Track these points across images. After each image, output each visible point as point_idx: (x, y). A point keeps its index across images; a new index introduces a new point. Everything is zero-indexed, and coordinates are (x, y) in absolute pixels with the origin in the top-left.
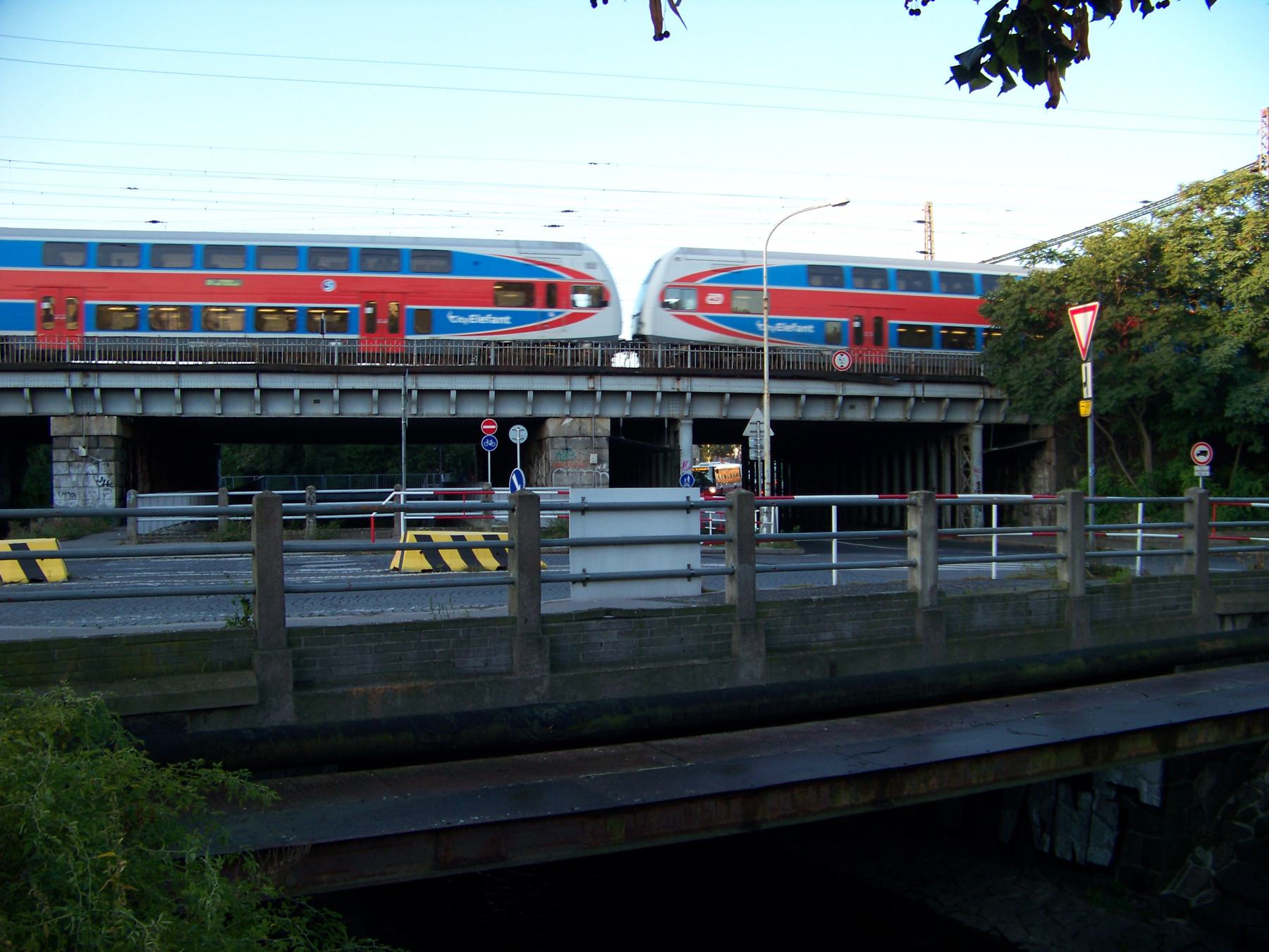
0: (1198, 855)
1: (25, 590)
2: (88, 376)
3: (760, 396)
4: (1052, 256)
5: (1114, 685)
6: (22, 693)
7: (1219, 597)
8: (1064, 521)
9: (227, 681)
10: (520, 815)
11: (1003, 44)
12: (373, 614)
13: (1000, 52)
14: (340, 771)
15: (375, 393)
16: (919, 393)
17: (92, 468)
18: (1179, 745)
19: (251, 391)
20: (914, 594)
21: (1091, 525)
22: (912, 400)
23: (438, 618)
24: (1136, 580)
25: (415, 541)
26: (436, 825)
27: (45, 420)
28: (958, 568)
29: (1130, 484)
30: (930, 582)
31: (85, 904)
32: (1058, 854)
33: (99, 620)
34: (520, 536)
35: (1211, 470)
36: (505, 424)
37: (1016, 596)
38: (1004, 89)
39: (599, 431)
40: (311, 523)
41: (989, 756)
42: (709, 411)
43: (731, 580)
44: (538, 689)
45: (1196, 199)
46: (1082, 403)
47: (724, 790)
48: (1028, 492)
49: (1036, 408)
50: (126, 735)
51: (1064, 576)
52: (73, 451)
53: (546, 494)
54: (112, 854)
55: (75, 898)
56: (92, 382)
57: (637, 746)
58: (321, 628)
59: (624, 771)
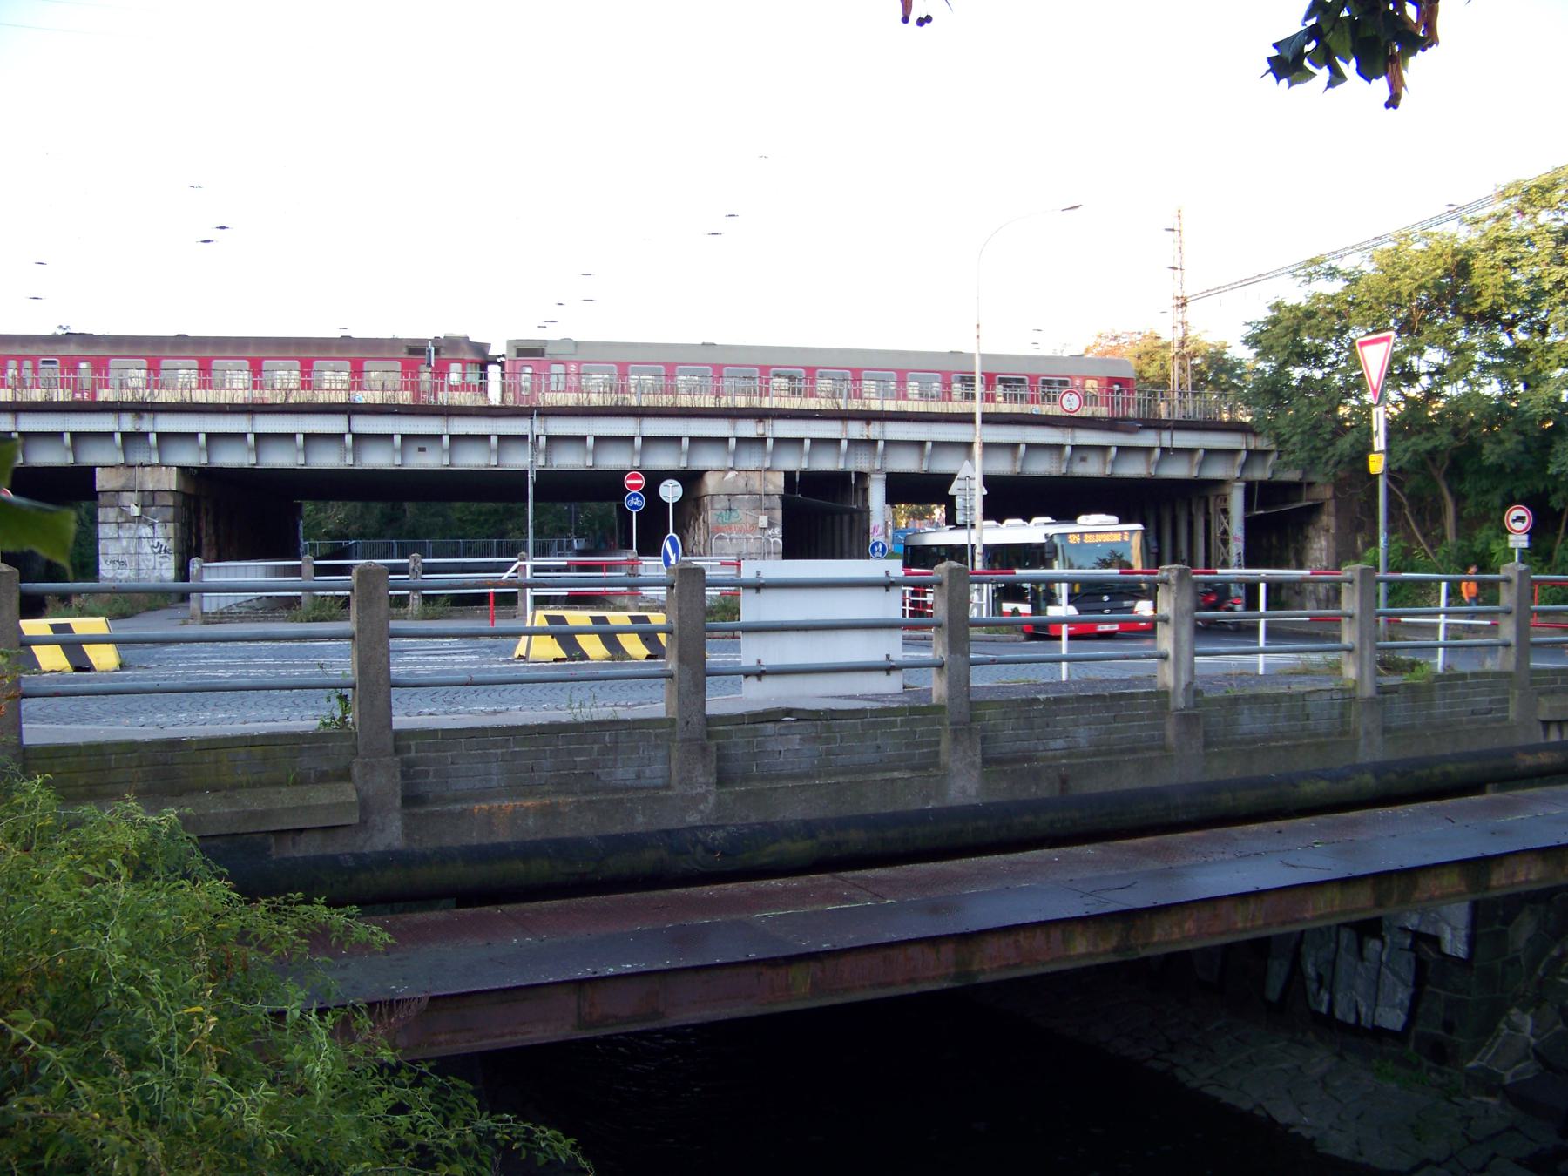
0: (1514, 1019)
1: (69, 680)
2: (141, 418)
3: (969, 445)
4: (1332, 273)
5: (1411, 808)
6: (86, 810)
7: (1542, 699)
8: (1350, 602)
9: (322, 795)
10: (683, 964)
11: (1332, 29)
12: (495, 712)
13: (1327, 39)
14: (458, 906)
15: (494, 440)
16: (1166, 444)
17: (146, 531)
18: (1494, 883)
19: (341, 436)
20: (1164, 694)
21: (1382, 609)
22: (1157, 452)
23: (580, 719)
24: (1439, 677)
25: (545, 624)
26: (580, 975)
27: (90, 472)
28: (1221, 662)
29: (1427, 557)
30: (1184, 678)
31: (170, 1068)
32: (1338, 1015)
33: (161, 718)
34: (680, 618)
35: (1530, 540)
36: (654, 479)
37: (1291, 696)
38: (1331, 84)
39: (771, 489)
40: (415, 600)
41: (1258, 894)
42: (906, 463)
43: (940, 674)
44: (701, 807)
45: (1515, 201)
46: (1372, 457)
47: (934, 934)
48: (1300, 566)
49: (1312, 462)
50: (204, 862)
51: (1350, 672)
52: (123, 510)
53: (712, 566)
54: (199, 1009)
55: (157, 1061)
56: (148, 424)
57: (824, 878)
58: (435, 731)
59: (807, 909)
